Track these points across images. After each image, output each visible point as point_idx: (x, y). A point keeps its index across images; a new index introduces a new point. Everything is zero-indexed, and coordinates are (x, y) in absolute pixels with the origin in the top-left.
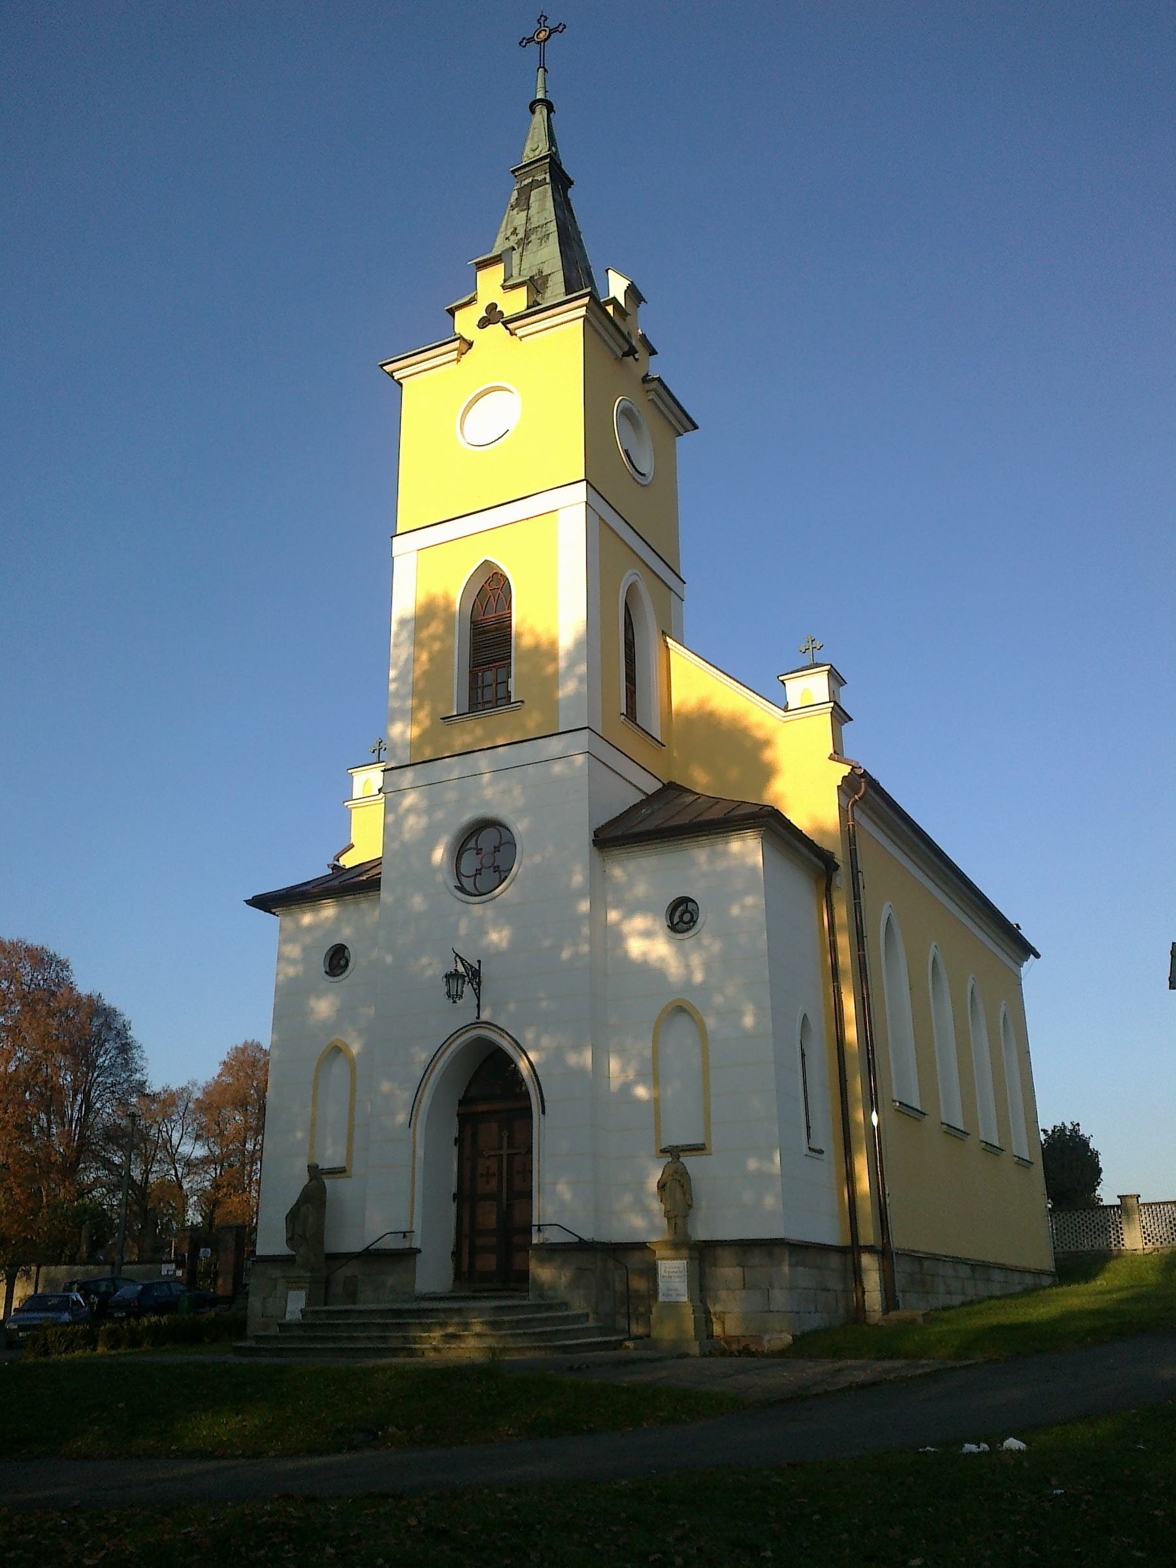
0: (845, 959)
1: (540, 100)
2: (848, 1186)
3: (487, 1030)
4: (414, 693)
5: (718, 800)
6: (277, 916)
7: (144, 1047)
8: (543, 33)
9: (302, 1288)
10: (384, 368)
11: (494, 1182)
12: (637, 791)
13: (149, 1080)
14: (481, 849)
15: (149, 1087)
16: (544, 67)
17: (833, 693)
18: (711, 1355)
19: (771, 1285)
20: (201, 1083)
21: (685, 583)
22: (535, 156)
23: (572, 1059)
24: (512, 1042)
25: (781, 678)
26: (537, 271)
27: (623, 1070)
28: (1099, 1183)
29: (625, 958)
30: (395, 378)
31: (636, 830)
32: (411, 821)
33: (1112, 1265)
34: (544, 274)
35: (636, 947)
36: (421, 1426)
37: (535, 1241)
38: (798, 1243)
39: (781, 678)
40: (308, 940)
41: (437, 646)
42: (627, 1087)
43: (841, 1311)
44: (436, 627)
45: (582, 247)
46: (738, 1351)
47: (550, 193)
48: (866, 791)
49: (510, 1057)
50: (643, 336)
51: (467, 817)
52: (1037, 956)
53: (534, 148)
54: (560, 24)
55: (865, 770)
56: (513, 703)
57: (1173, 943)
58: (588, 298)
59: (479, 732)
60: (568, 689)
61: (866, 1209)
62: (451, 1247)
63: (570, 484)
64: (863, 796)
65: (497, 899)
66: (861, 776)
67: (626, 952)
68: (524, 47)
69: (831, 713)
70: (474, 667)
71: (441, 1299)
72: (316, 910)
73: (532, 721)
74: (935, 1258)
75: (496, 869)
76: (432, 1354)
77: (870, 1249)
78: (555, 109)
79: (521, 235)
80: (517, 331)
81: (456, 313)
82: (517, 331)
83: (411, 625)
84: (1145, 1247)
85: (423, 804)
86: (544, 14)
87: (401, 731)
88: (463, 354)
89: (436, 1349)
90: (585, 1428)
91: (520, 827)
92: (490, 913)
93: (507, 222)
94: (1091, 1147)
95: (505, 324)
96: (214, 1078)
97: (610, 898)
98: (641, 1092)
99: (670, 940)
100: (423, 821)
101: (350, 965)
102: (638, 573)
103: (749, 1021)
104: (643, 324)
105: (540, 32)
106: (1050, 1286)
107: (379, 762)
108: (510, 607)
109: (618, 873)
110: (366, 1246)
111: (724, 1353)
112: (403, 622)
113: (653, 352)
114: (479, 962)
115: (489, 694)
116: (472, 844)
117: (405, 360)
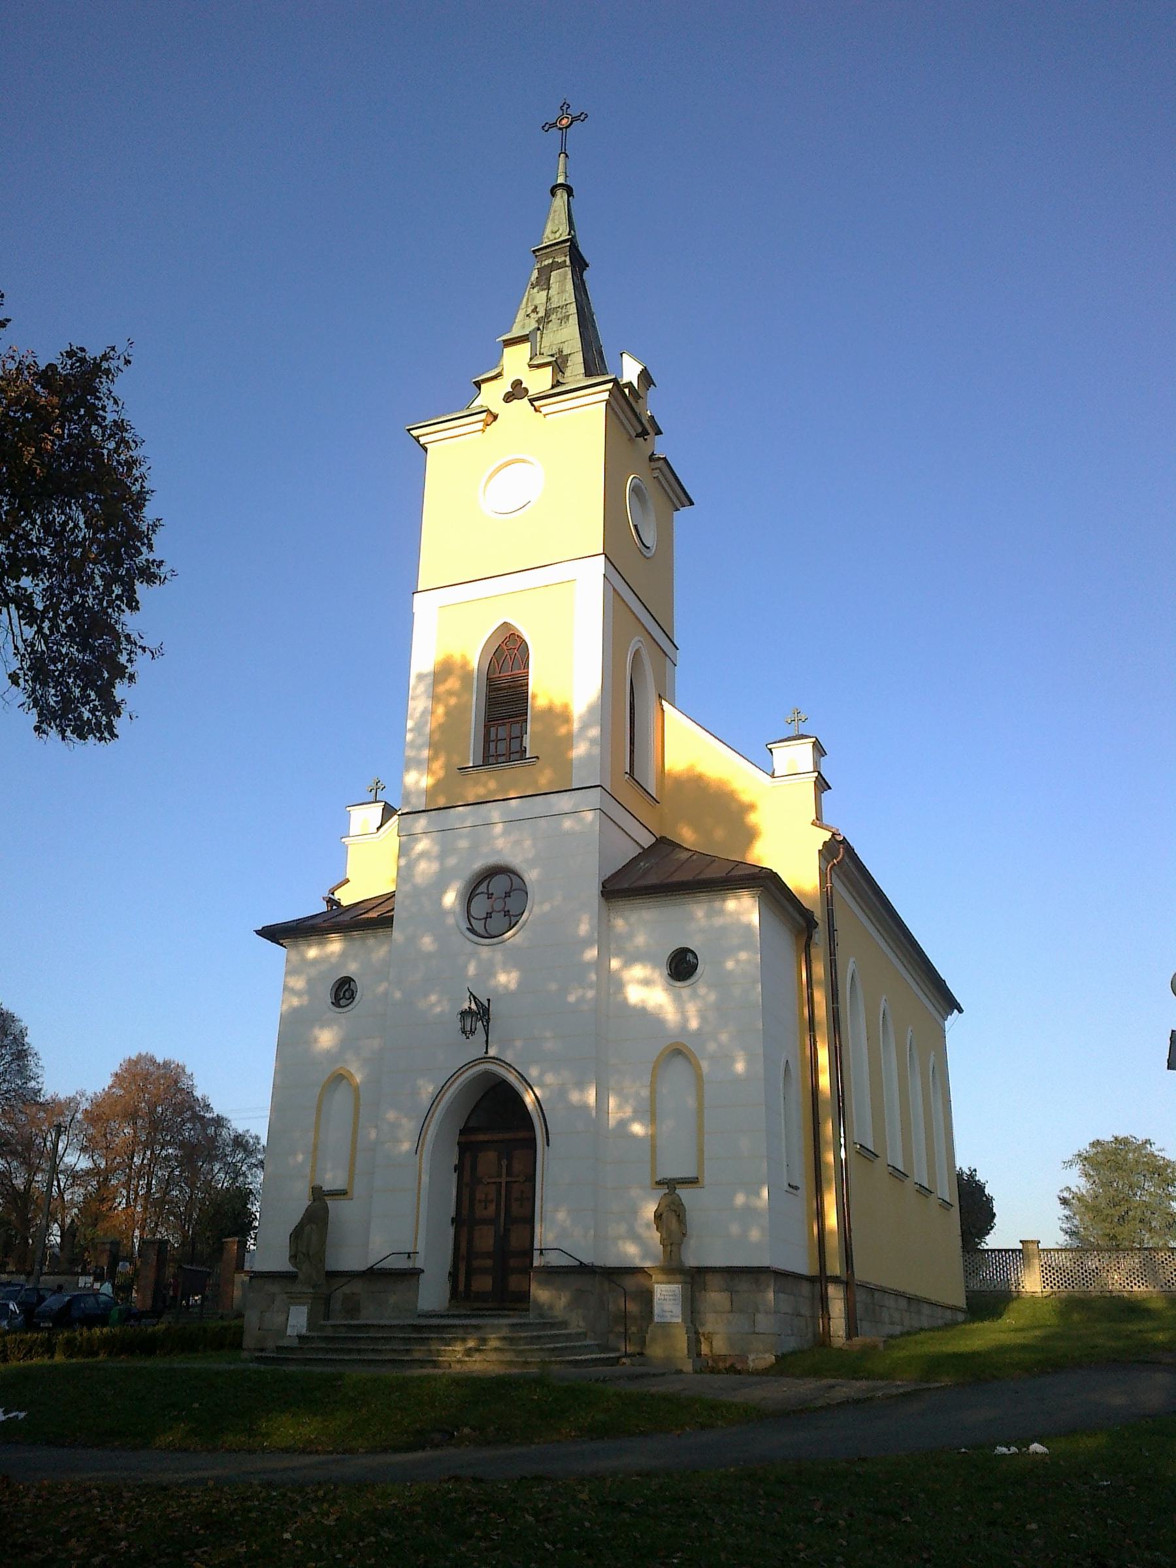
0: (821, 1012)
1: (561, 185)
2: (818, 1222)
3: (490, 1064)
4: (432, 745)
5: (714, 858)
6: (285, 947)
7: (41, 1055)
8: (566, 120)
9: (303, 1304)
10: (411, 432)
11: (492, 1208)
12: (634, 843)
13: (45, 1089)
14: (492, 894)
15: (44, 1096)
16: (565, 153)
17: (816, 764)
18: (701, 1372)
19: (757, 1310)
20: (90, 1093)
21: (678, 649)
22: (555, 239)
23: (575, 1097)
24: (519, 1077)
25: (769, 746)
26: (557, 350)
27: (620, 1107)
28: (992, 1227)
29: (625, 1003)
30: (421, 443)
31: (636, 884)
32: (423, 866)
33: (1014, 1305)
34: (565, 353)
35: (635, 994)
36: (492, 1428)
37: (536, 1264)
39: (769, 746)
40: (313, 972)
41: (453, 701)
42: (623, 1124)
43: (810, 1335)
44: (452, 683)
45: (594, 327)
46: (726, 1369)
47: (570, 276)
48: (843, 856)
49: (513, 1088)
50: (652, 417)
51: (478, 865)
52: (960, 1011)
53: (554, 230)
54: (582, 113)
55: (844, 838)
56: (529, 758)
57: (1173, 1031)
58: (612, 384)
59: (492, 785)
60: (580, 750)
61: (833, 1243)
62: (448, 1266)
64: (841, 860)
65: (507, 943)
66: (840, 842)
67: (625, 999)
68: (546, 131)
69: (815, 782)
70: (489, 721)
71: (442, 1316)
72: (322, 944)
73: (545, 779)
74: (884, 1291)
75: (507, 913)
76: (458, 1366)
77: (836, 1280)
78: (574, 193)
79: (542, 313)
80: (541, 409)
81: (482, 386)
82: (541, 409)
83: (429, 680)
84: (1044, 1290)
85: (436, 850)
86: (568, 102)
87: (418, 780)
88: (488, 425)
89: (459, 1361)
90: (637, 1431)
91: (531, 876)
92: (499, 957)
93: (528, 299)
94: (986, 1193)
95: (531, 401)
96: (104, 1090)
97: (613, 946)
98: (637, 1129)
99: (669, 989)
100: (434, 867)
101: (357, 998)
102: (642, 639)
103: (740, 1067)
104: (651, 407)
105: (563, 119)
106: (964, 1322)
107: (376, 802)
108: (526, 666)
109: (620, 924)
110: (369, 1266)
111: (713, 1371)
112: (421, 677)
113: (659, 432)
114: (489, 1000)
115: (502, 747)
116: (483, 888)
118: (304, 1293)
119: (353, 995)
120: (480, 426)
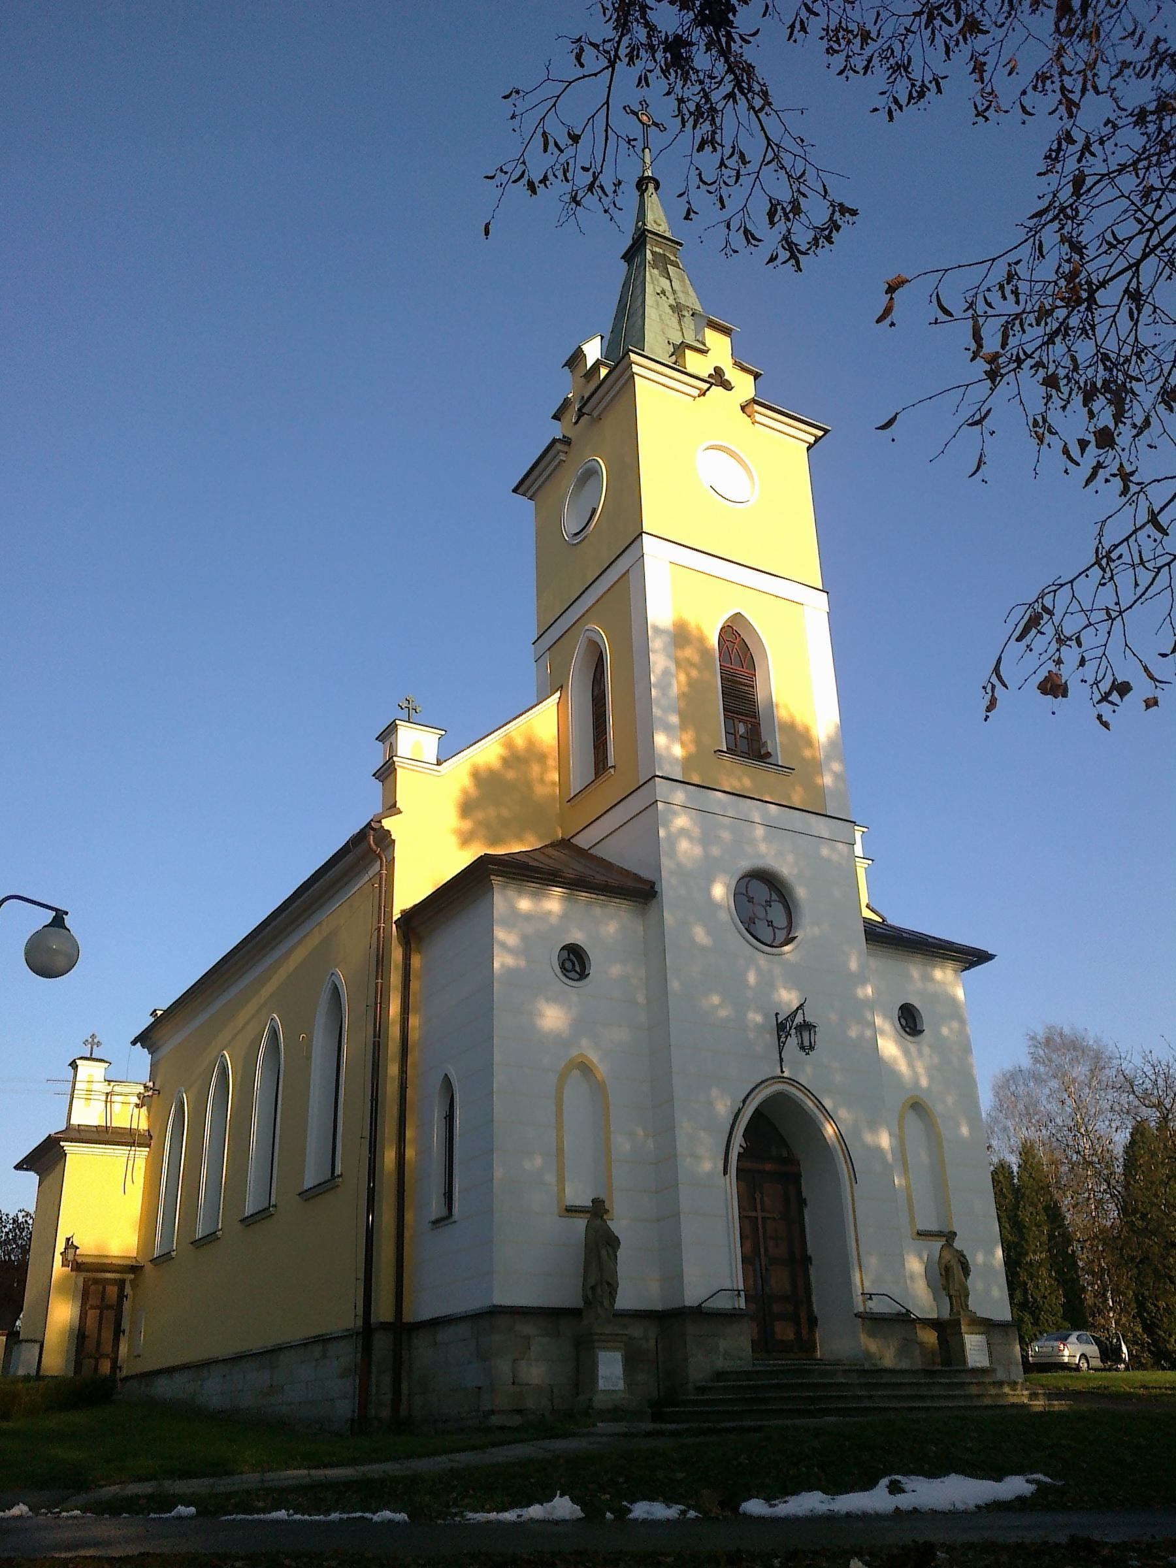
23: (868, 1138)
38: (725, 1312)
59: (747, 782)
63: (676, 543)
72: (536, 896)
117: (653, 363)
118: (617, 1335)
119: (565, 969)
120: (696, 392)
